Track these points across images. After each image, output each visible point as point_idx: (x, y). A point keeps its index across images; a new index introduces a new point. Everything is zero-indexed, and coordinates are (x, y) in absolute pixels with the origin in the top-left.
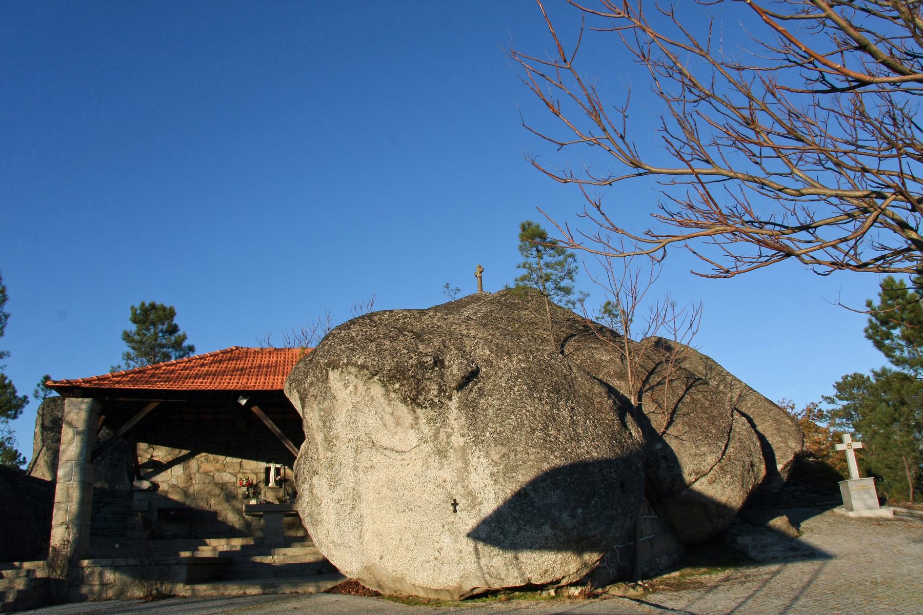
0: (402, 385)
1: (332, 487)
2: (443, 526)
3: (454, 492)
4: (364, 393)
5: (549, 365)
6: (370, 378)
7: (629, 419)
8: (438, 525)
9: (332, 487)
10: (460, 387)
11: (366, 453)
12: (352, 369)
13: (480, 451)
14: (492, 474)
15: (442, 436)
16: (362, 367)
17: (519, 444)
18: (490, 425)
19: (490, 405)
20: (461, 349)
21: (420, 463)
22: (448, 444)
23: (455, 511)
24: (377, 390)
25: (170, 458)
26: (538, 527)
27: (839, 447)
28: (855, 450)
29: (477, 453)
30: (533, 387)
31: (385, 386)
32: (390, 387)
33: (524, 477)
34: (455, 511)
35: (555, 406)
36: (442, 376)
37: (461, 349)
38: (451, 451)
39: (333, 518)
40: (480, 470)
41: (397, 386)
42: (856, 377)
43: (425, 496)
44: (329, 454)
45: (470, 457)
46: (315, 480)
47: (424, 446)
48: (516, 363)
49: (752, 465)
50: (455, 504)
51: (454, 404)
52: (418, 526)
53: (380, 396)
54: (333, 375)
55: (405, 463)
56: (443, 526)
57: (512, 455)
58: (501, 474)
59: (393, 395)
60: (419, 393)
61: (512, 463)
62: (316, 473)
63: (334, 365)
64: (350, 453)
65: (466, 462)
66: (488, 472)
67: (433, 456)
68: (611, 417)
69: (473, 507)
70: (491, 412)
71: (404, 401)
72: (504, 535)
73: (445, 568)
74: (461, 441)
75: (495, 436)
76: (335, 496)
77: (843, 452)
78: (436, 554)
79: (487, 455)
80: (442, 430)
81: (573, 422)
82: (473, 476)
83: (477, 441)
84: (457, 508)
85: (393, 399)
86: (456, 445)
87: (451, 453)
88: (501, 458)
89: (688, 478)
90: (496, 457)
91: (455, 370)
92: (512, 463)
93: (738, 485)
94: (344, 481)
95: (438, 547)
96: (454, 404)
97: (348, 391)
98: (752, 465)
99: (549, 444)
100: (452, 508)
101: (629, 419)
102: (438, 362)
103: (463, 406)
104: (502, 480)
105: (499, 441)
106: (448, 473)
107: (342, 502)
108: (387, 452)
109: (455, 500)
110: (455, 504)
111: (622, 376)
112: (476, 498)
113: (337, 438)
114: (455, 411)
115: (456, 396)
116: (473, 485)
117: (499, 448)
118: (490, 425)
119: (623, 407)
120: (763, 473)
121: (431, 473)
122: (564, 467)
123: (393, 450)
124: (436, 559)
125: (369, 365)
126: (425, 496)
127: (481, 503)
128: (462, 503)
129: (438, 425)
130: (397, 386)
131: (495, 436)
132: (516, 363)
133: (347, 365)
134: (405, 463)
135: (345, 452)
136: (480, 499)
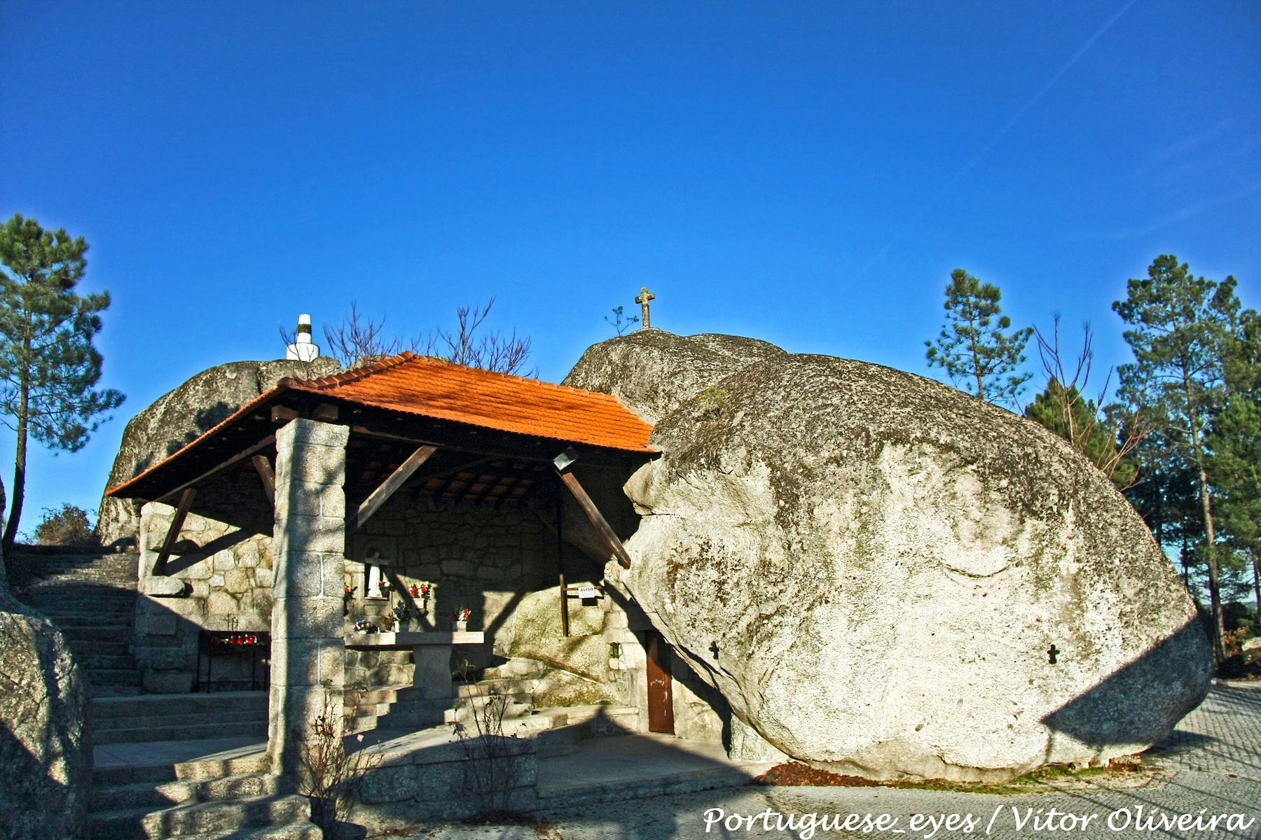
0: (1011, 483)
1: (854, 624)
2: (1031, 682)
3: (1054, 635)
4: (940, 485)
6: (960, 466)
8: (1021, 679)
9: (854, 624)
12: (927, 448)
13: (1105, 582)
14: (1121, 615)
15: (1047, 558)
16: (949, 447)
17: (1158, 578)
18: (1118, 549)
21: (1006, 593)
22: (1054, 570)
23: (1053, 661)
24: (967, 484)
25: (212, 536)
26: (1168, 684)
29: (1100, 586)
31: (984, 481)
32: (993, 483)
33: (1170, 623)
34: (1053, 661)
38: (1056, 579)
39: (843, 669)
40: (1103, 607)
41: (1004, 483)
42: (1161, 256)
43: (1005, 641)
44: (857, 572)
45: (1087, 589)
47: (1014, 571)
50: (1053, 652)
52: (990, 682)
53: (968, 494)
54: (891, 455)
55: (981, 592)
56: (1031, 682)
57: (1152, 591)
58: (1135, 615)
59: (994, 495)
60: (1034, 497)
61: (1152, 601)
63: (899, 438)
66: (1116, 610)
67: (1027, 584)
69: (1086, 657)
70: (1113, 532)
71: (1012, 506)
72: (1125, 693)
73: (1022, 740)
74: (1074, 568)
75: (1127, 564)
76: (855, 638)
78: (1012, 720)
79: (1117, 588)
80: (1047, 550)
82: (1090, 615)
83: (1099, 569)
84: (1058, 657)
85: (992, 502)
86: (1064, 572)
87: (1057, 584)
88: (1137, 594)
90: (1130, 593)
92: (1152, 601)
94: (880, 615)
95: (1015, 709)
97: (914, 480)
100: (1048, 657)
104: (1136, 622)
106: (1046, 608)
107: (866, 647)
108: (955, 576)
109: (1053, 647)
110: (1053, 652)
112: (1090, 644)
113: (880, 548)
114: (1071, 527)
116: (1088, 627)
117: (1134, 580)
118: (1118, 549)
121: (1020, 609)
123: (963, 573)
124: (1010, 726)
125: (961, 445)
126: (1005, 641)
127: (1098, 652)
129: (1044, 543)
130: (1004, 483)
131: (1127, 564)
133: (921, 441)
134: (981, 592)
135: (887, 570)
136: (1098, 647)
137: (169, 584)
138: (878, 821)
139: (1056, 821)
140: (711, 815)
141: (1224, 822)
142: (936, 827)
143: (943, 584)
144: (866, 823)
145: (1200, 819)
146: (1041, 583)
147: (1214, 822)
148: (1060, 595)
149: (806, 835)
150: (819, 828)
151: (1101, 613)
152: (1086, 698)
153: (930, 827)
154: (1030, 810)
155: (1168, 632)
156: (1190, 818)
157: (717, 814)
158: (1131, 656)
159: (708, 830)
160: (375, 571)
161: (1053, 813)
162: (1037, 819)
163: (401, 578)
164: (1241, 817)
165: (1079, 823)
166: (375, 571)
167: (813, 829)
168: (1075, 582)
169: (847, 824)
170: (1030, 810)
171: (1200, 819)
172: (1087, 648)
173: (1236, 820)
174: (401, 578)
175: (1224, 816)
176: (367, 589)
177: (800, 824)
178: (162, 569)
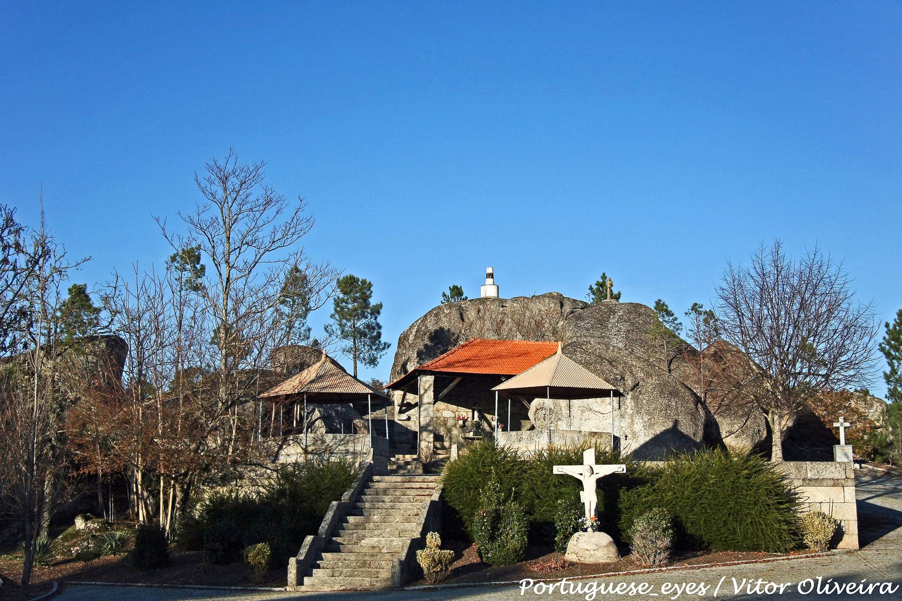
5: (668, 382)
7: (699, 405)
10: (631, 390)
11: (587, 413)
19: (644, 399)
20: (631, 372)
27: (835, 425)
28: (845, 428)
30: (661, 392)
33: (659, 430)
35: (669, 401)
36: (624, 384)
37: (631, 372)
46: (559, 422)
48: (653, 381)
49: (759, 431)
51: (629, 397)
62: (560, 419)
64: (580, 413)
65: (633, 421)
68: (692, 405)
70: (644, 401)
77: (838, 428)
81: (677, 408)
82: (635, 426)
83: (638, 412)
89: (723, 435)
91: (630, 383)
93: (750, 440)
96: (629, 397)
98: (759, 431)
99: (667, 417)
101: (699, 405)
102: (623, 378)
103: (633, 398)
105: (648, 413)
111: (698, 382)
115: (630, 393)
119: (698, 400)
120: (765, 435)
122: (651, 440)
128: (629, 436)
132: (653, 381)
137: (404, 416)
138: (640, 588)
139: (763, 586)
140: (524, 583)
141: (878, 588)
142: (679, 592)
143: (592, 415)
144: (631, 589)
145: (861, 587)
146: (622, 416)
147: (871, 588)
148: (628, 420)
149: (591, 597)
150: (598, 593)
151: (638, 426)
152: (635, 451)
153: (675, 593)
154: (744, 580)
155: (658, 432)
156: (855, 585)
157: (528, 583)
158: (647, 439)
159: (522, 594)
160: (476, 413)
161: (760, 582)
162: (749, 586)
163: (486, 415)
164: (890, 585)
165: (778, 589)
166: (476, 413)
167: (594, 593)
168: (632, 415)
169: (618, 589)
170: (744, 580)
171: (861, 587)
172: (635, 435)
173: (886, 586)
174: (486, 415)
175: (878, 584)
176: (473, 418)
177: (586, 590)
178: (401, 412)
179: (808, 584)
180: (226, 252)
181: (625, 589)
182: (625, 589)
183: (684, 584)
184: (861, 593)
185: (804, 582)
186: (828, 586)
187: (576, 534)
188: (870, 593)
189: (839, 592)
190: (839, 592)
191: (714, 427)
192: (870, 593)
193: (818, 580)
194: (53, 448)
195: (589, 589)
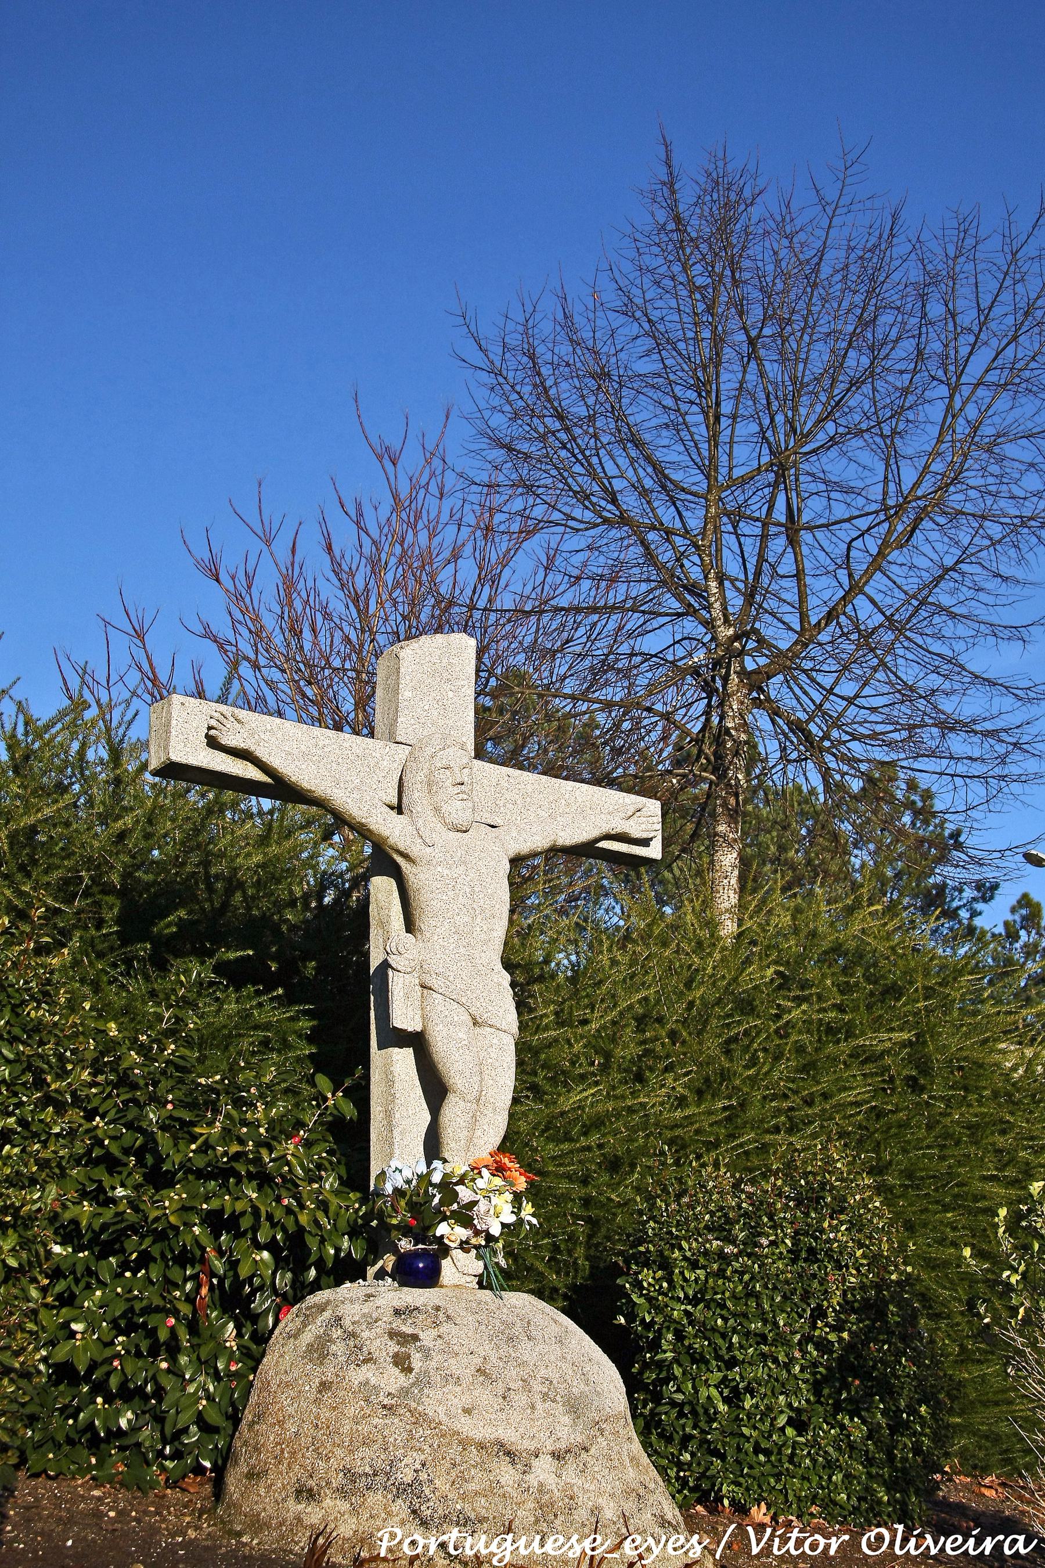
147: (988, 1545)
164: (1022, 1538)
165: (828, 1546)
169: (549, 1547)
173: (1015, 1542)
179: (880, 1538)
180: (491, 380)
181: (959, 1547)
182: (959, 1547)
183: (942, 1539)
184: (971, 1552)
185: (873, 1534)
186: (913, 1541)
187: (282, 1359)
188: (987, 1553)
189: (934, 1551)
190: (934, 1551)
191: (359, 1071)
192: (987, 1553)
193: (896, 1530)
194: (663, 1044)
195: (499, 1545)
